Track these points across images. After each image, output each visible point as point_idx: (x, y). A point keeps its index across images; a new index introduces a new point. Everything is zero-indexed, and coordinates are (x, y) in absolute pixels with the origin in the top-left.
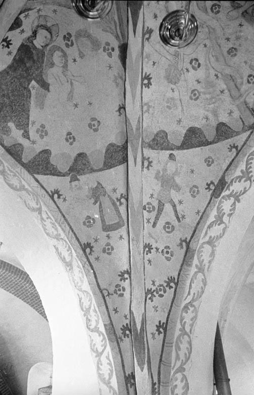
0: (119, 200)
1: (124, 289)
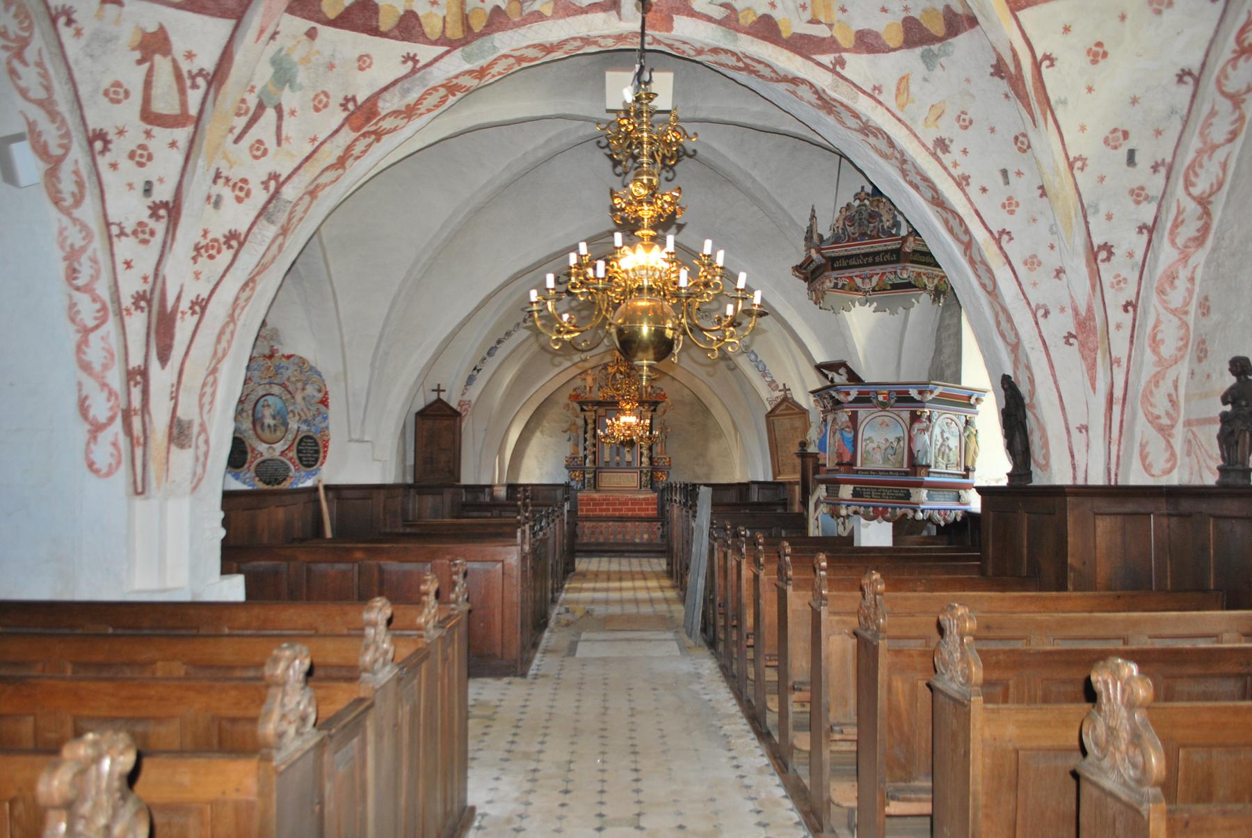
0: (193, 77)
1: (152, 233)
